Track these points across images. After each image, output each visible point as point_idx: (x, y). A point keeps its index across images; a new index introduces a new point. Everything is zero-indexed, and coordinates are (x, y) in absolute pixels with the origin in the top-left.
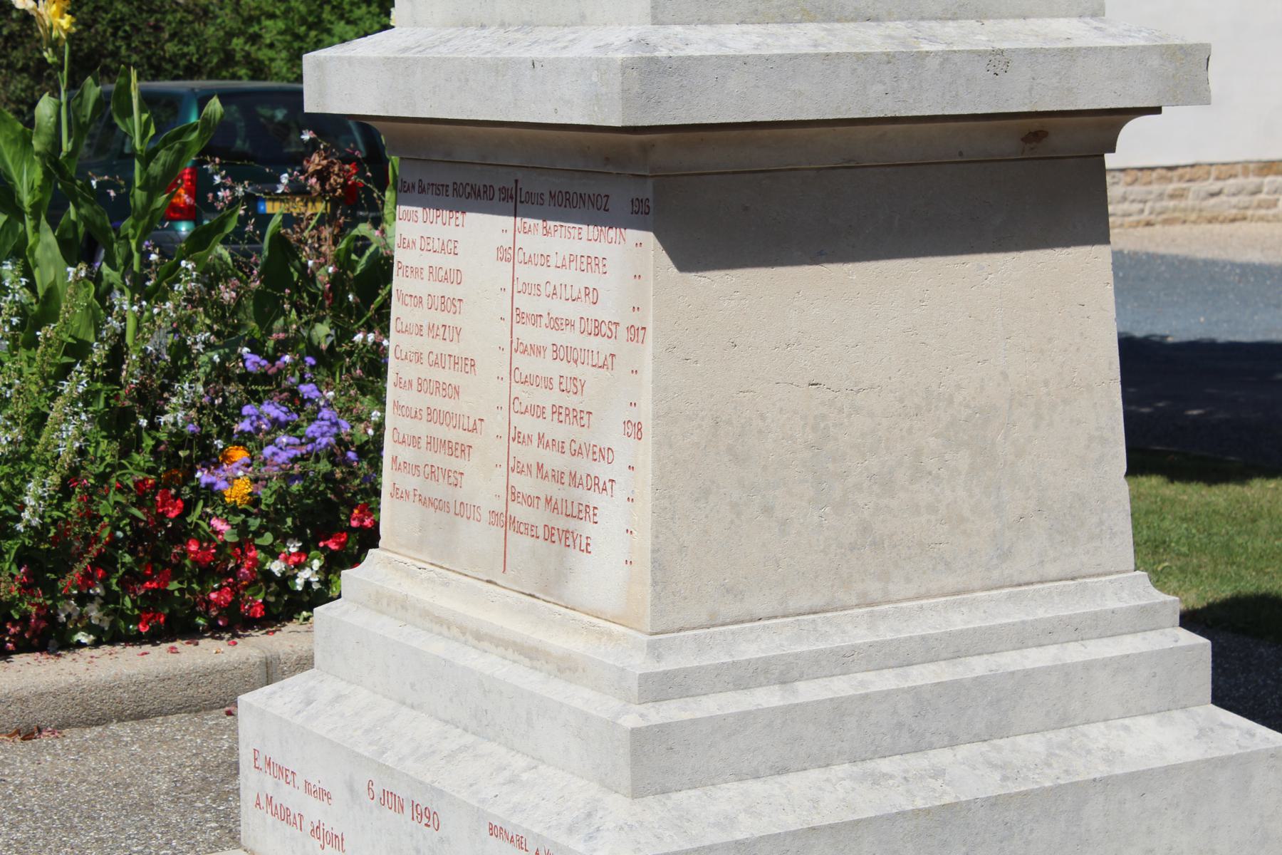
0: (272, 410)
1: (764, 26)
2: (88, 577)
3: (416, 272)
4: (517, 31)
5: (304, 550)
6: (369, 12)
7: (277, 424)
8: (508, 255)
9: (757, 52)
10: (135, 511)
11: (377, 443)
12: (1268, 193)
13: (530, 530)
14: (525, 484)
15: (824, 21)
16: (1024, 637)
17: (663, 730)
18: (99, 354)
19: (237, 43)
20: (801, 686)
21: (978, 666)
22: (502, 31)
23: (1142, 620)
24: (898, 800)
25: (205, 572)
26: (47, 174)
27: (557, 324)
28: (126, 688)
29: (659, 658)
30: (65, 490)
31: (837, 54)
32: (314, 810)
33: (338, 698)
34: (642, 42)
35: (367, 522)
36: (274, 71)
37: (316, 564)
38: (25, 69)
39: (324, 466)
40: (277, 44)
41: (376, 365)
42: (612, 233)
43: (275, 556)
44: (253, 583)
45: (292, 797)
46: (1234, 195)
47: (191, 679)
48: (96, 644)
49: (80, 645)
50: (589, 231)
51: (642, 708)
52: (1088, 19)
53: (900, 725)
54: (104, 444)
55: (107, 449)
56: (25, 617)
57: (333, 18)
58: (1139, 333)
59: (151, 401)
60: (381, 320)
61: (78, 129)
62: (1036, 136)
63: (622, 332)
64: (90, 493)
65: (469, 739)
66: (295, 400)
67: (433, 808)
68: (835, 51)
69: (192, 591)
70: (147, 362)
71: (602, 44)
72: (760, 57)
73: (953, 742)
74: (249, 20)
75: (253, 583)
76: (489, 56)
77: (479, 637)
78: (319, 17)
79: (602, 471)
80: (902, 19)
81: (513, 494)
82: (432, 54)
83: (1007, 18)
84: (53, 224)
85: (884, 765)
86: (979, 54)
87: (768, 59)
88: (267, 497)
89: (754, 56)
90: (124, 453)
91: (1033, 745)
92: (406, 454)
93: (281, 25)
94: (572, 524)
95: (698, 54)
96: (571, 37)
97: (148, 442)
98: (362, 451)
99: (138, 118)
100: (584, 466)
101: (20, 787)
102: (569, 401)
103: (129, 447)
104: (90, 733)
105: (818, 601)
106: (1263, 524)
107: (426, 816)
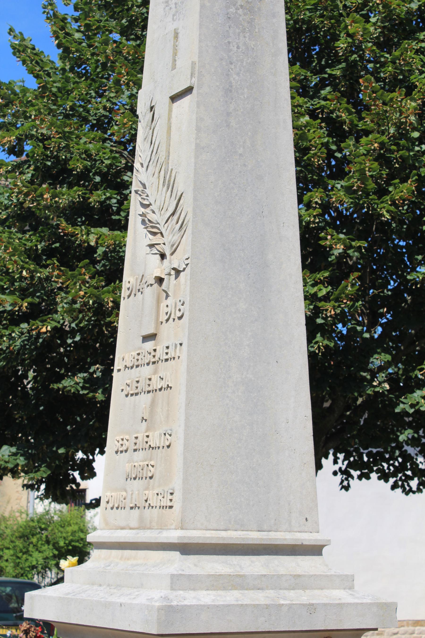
1: (216, 591)
4: (114, 588)
6: (48, 548)
9: (213, 604)
12: (417, 634)
15: (241, 590)
22: (108, 588)
31: (246, 604)
34: (166, 598)
36: (7, 571)
40: (9, 560)
46: (403, 634)
52: (347, 590)
57: (34, 550)
68: (245, 603)
71: (150, 598)
72: (215, 605)
76: (103, 600)
78: (27, 549)
80: (272, 589)
83: (315, 589)
86: (304, 605)
87: (218, 606)
89: (212, 605)
93: (12, 552)
95: (189, 604)
96: (137, 593)
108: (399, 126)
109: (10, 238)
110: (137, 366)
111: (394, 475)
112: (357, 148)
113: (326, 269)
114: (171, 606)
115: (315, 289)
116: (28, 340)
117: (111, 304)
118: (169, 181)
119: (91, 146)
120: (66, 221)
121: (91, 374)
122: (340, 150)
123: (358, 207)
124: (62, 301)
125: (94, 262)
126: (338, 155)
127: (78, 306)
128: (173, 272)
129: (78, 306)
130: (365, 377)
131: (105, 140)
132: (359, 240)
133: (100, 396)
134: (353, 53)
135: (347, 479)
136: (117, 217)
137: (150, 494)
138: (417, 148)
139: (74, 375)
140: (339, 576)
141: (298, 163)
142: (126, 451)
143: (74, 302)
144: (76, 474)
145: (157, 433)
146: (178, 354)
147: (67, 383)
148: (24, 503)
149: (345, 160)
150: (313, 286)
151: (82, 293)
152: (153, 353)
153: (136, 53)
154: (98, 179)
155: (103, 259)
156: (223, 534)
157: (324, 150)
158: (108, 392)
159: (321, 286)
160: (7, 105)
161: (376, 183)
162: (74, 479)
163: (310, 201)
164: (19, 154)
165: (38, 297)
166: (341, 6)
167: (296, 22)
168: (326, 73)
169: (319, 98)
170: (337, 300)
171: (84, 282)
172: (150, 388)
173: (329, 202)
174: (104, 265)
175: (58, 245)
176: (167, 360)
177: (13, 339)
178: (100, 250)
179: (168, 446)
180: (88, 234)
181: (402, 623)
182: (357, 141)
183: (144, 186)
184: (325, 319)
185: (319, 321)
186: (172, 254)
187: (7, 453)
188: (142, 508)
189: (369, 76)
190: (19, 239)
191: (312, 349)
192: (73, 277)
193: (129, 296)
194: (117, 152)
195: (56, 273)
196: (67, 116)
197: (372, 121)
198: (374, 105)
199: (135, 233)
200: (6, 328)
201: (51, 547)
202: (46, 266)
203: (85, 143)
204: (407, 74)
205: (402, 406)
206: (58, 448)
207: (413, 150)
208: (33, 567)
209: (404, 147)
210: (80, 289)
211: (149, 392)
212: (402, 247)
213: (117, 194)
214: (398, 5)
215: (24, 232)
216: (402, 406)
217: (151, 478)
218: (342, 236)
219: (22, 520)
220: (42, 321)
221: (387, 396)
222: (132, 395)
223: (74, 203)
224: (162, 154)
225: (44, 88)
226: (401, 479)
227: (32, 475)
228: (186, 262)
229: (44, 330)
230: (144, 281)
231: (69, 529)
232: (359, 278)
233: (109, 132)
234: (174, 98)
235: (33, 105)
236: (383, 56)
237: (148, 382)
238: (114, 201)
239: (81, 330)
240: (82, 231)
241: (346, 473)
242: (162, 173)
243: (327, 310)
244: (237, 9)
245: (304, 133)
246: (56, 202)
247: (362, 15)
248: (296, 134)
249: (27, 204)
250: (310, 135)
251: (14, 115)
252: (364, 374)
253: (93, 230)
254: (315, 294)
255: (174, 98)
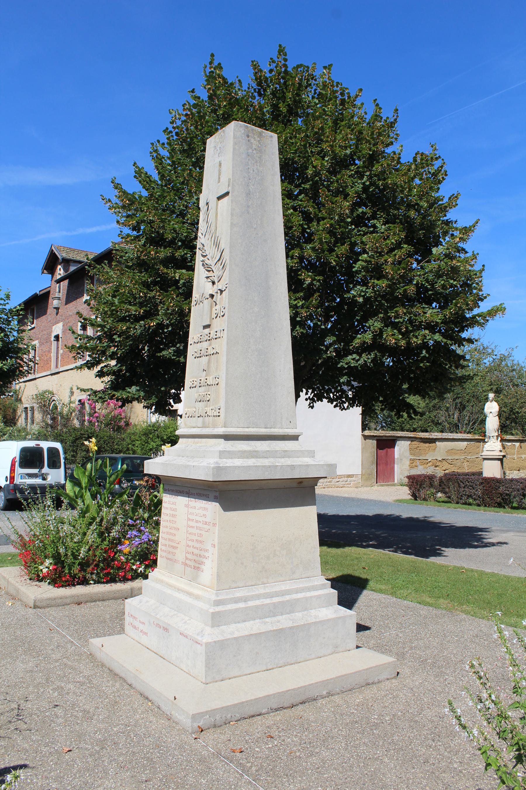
0: (135, 533)
2: (93, 569)
3: (167, 508)
5: (140, 564)
7: (136, 536)
8: (187, 506)
10: (104, 555)
11: (158, 541)
13: (190, 566)
14: (189, 556)
16: (297, 591)
17: (219, 612)
18: (98, 520)
19: (130, 446)
20: (249, 602)
21: (287, 598)
23: (323, 587)
24: (270, 628)
25: (119, 568)
26: (88, 480)
27: (197, 522)
28: (101, 594)
29: (218, 596)
30: (89, 550)
32: (141, 627)
33: (147, 602)
34: (217, 463)
35: (155, 558)
37: (143, 567)
38: (85, 450)
39: (145, 545)
41: (158, 523)
42: (210, 503)
43: (134, 565)
44: (129, 571)
45: (136, 623)
47: (114, 592)
48: (95, 584)
49: (91, 584)
50: (204, 502)
51: (214, 608)
53: (270, 611)
54: (98, 539)
55: (99, 540)
56: (79, 577)
58: (322, 513)
59: (108, 530)
60: (159, 514)
61: (96, 470)
62: (301, 482)
63: (211, 524)
64: (94, 550)
65: (176, 612)
66: (140, 531)
67: (168, 628)
69: (116, 572)
70: (108, 522)
73: (282, 614)
74: (133, 441)
75: (129, 571)
77: (179, 590)
79: (206, 554)
81: (187, 558)
82: (172, 462)
84: (89, 490)
85: (267, 620)
87: (244, 467)
88: (133, 552)
90: (102, 541)
91: (299, 615)
92: (164, 548)
93: (139, 442)
94: (199, 566)
97: (107, 539)
98: (154, 542)
99: (108, 468)
100: (202, 553)
101: (76, 616)
102: (200, 539)
103: (103, 540)
104: (92, 604)
105: (253, 583)
106: (348, 558)
107: (166, 629)
108: (340, 215)
109: (134, 276)
110: (201, 342)
111: (336, 400)
112: (318, 227)
113: (301, 291)
114: (220, 467)
115: (296, 302)
116: (144, 330)
117: (187, 310)
118: (217, 243)
119: (176, 226)
120: (163, 267)
121: (178, 348)
122: (309, 228)
123: (319, 259)
124: (161, 309)
125: (178, 288)
126: (309, 231)
127: (170, 311)
128: (219, 292)
129: (170, 311)
130: (322, 349)
131: (184, 223)
132: (319, 276)
133: (182, 359)
134: (316, 176)
135: (312, 403)
136: (190, 264)
137: (208, 409)
138: (350, 227)
139: (169, 348)
140: (307, 451)
141: (286, 234)
142: (195, 387)
143: (168, 309)
144: (171, 401)
145: (211, 377)
146: (222, 335)
147: (164, 353)
148: (145, 417)
149: (311, 234)
150: (295, 300)
151: (172, 304)
152: (209, 335)
153: (200, 176)
154: (180, 244)
155: (183, 287)
156: (247, 430)
157: (300, 227)
158: (185, 357)
159: (299, 300)
160: (131, 204)
161: (329, 246)
162: (170, 403)
163: (293, 255)
164: (139, 230)
165: (149, 307)
166: (309, 151)
167: (286, 159)
168: (301, 187)
169: (298, 200)
170: (307, 308)
171: (173, 299)
172: (207, 354)
173: (303, 255)
174: (183, 290)
175: (159, 279)
176: (216, 338)
177: (136, 329)
178: (182, 282)
179: (217, 384)
180: (175, 273)
181: (341, 476)
182: (318, 223)
183: (203, 245)
184: (301, 318)
185: (298, 319)
186: (218, 282)
187: (135, 390)
188: (204, 417)
189: (324, 188)
190: (139, 276)
191: (294, 334)
192: (167, 296)
193: (196, 305)
194: (190, 229)
195: (158, 294)
196: (164, 210)
197: (326, 213)
198: (327, 204)
199: (199, 271)
200: (132, 324)
201: (160, 439)
202: (152, 291)
203: (173, 224)
204: (344, 188)
205: (341, 363)
206: (161, 387)
207: (347, 228)
208: (151, 450)
209: (343, 226)
210: (171, 302)
211: (207, 356)
212: (342, 280)
213: (191, 252)
214: (340, 151)
215: (141, 273)
216: (341, 363)
217: (208, 401)
218: (310, 274)
219: (144, 425)
220: (151, 320)
221: (334, 359)
222: (198, 357)
223: (168, 257)
224: (213, 228)
225: (152, 195)
226: (339, 402)
227: (148, 401)
228: (226, 286)
229: (152, 324)
230: (204, 297)
231: (169, 430)
232: (319, 296)
233: (186, 218)
234: (219, 198)
235: (145, 204)
236: (332, 178)
237: (206, 350)
238: (189, 255)
239: (171, 325)
240: (171, 271)
241: (313, 400)
242: (213, 238)
243: (302, 313)
244: (253, 150)
245: (290, 219)
246: (158, 256)
247: (320, 156)
248: (285, 219)
249: (142, 257)
250: (293, 220)
251: (135, 210)
252: (322, 347)
253: (177, 271)
254: (296, 304)
255: (219, 198)
